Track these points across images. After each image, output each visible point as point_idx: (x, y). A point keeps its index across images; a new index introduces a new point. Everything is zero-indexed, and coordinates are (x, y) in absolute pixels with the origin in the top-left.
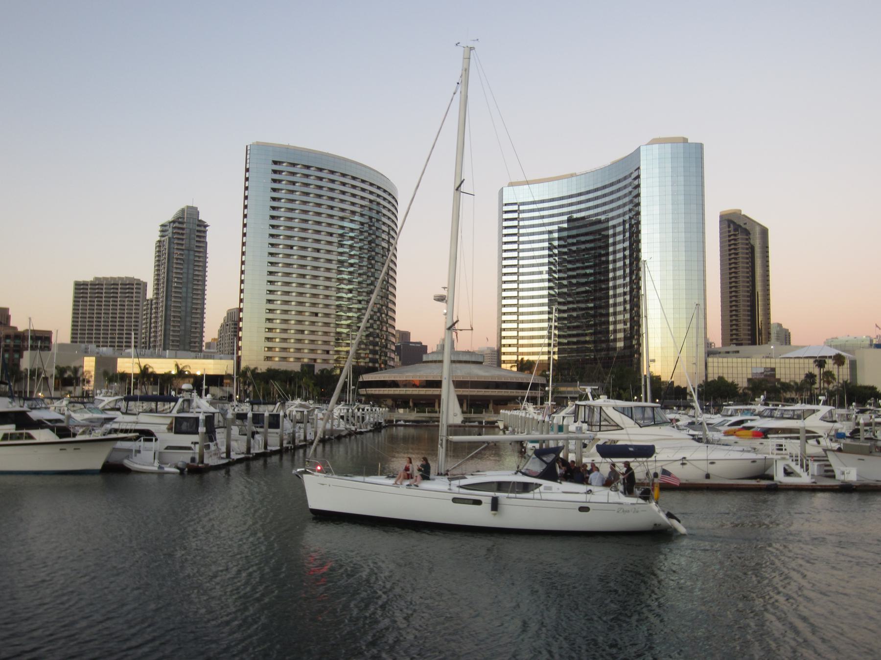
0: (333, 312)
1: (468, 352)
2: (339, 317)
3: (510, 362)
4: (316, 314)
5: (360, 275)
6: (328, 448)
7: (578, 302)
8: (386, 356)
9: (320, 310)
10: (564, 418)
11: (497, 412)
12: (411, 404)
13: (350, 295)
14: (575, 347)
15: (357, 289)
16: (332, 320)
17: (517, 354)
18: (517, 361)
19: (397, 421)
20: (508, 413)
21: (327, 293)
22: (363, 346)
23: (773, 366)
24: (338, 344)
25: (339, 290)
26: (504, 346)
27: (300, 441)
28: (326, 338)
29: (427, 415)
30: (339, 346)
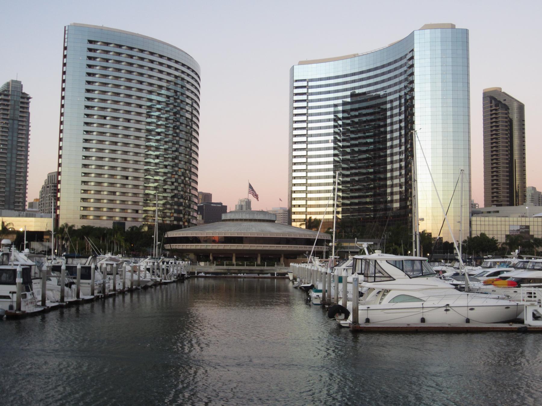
0: (142, 175)
1: (262, 212)
2: (147, 180)
3: (299, 220)
4: (127, 178)
7: (360, 168)
8: (189, 215)
11: (287, 265)
12: (211, 258)
13: (157, 161)
14: (357, 207)
15: (163, 155)
16: (141, 183)
17: (306, 213)
19: (198, 273)
20: (297, 265)
23: (527, 224)
25: (147, 156)
26: (294, 206)
27: (110, 291)
28: (135, 199)
29: (225, 267)
30: (147, 206)
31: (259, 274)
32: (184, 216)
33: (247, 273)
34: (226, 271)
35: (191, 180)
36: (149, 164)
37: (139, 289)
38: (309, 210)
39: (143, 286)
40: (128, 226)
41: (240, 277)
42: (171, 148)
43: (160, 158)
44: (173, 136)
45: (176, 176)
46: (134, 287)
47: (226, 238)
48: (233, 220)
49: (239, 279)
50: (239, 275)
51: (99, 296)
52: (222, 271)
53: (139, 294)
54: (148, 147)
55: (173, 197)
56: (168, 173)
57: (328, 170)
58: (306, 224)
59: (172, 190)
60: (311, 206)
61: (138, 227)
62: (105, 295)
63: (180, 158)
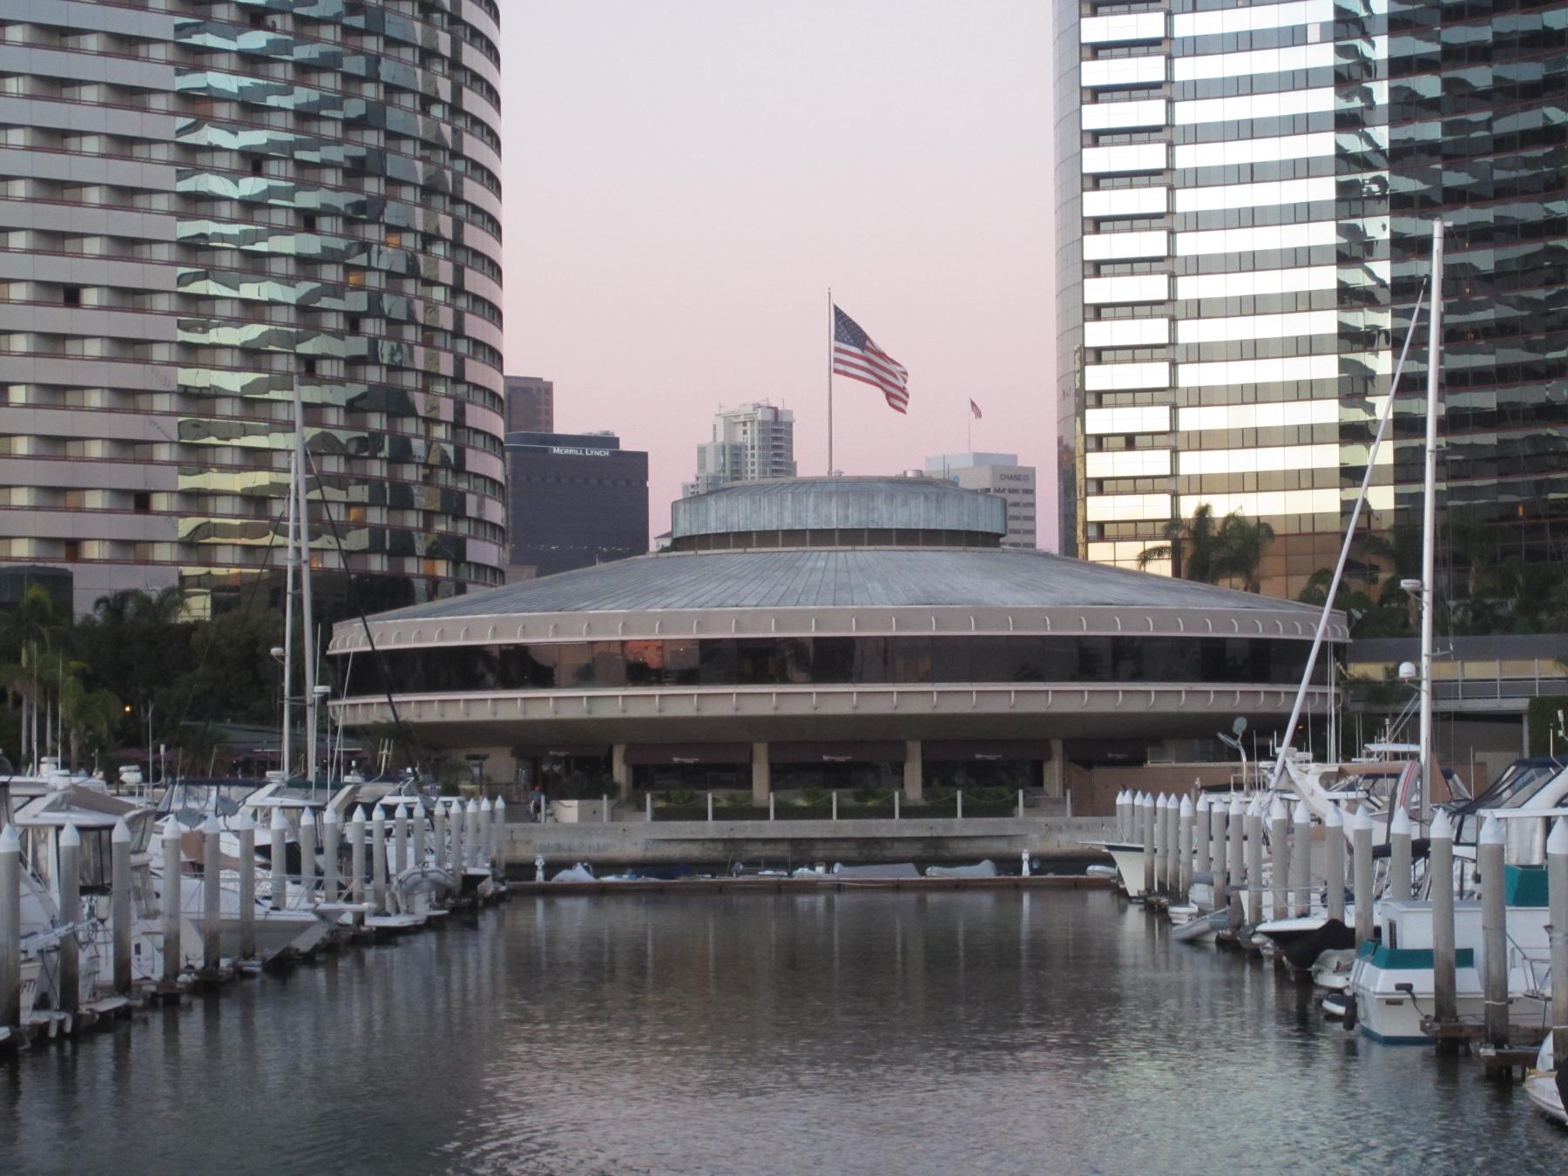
0: (164, 278)
1: (920, 485)
2: (196, 309)
3: (1134, 530)
4: (71, 295)
5: (304, 69)
6: (230, 1017)
7: (1503, 192)
8: (458, 514)
9: (90, 268)
10: (1549, 823)
11: (1096, 805)
12: (620, 773)
13: (251, 186)
14: (1489, 439)
15: (286, 151)
16: (158, 325)
17: (1172, 484)
18: (1174, 523)
19: (553, 867)
21: (125, 173)
22: (332, 465)
24: (196, 457)
25: (191, 157)
26: (1099, 442)
27: (99, 992)
28: (130, 426)
29: (711, 828)
30: (203, 467)
31: (921, 864)
32: (428, 526)
33: (847, 863)
34: (717, 852)
35: (462, 303)
36: (203, 208)
37: (252, 975)
38: (1191, 463)
39: (270, 953)
40: (91, 589)
41: (810, 887)
42: (337, 104)
43: (272, 167)
44: (348, 31)
45: (373, 280)
46: (224, 963)
47: (709, 649)
48: (742, 539)
49: (803, 901)
50: (803, 873)
51: (43, 1028)
52: (695, 851)
53: (247, 1005)
54: (196, 104)
55: (353, 408)
56: (329, 256)
57: (1305, 213)
58: (1176, 553)
59: (353, 362)
60: (1202, 441)
61: (154, 596)
62: (77, 1019)
63: (394, 167)
